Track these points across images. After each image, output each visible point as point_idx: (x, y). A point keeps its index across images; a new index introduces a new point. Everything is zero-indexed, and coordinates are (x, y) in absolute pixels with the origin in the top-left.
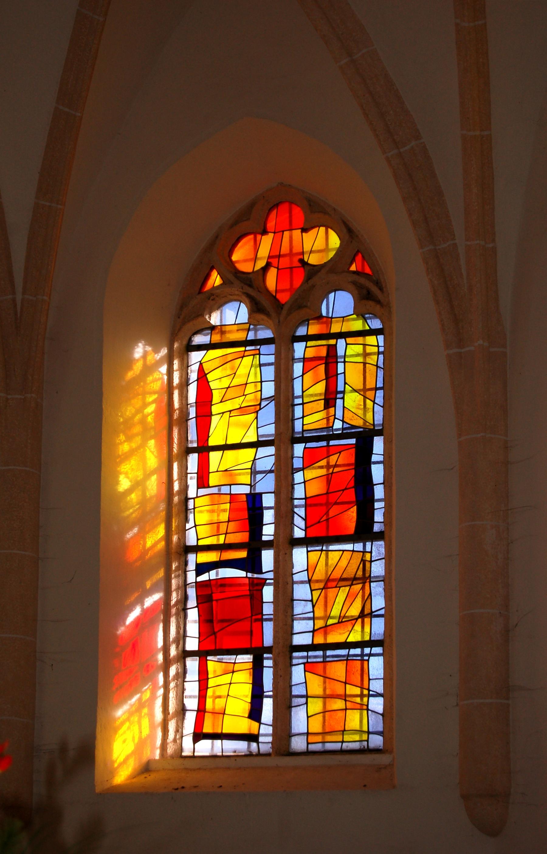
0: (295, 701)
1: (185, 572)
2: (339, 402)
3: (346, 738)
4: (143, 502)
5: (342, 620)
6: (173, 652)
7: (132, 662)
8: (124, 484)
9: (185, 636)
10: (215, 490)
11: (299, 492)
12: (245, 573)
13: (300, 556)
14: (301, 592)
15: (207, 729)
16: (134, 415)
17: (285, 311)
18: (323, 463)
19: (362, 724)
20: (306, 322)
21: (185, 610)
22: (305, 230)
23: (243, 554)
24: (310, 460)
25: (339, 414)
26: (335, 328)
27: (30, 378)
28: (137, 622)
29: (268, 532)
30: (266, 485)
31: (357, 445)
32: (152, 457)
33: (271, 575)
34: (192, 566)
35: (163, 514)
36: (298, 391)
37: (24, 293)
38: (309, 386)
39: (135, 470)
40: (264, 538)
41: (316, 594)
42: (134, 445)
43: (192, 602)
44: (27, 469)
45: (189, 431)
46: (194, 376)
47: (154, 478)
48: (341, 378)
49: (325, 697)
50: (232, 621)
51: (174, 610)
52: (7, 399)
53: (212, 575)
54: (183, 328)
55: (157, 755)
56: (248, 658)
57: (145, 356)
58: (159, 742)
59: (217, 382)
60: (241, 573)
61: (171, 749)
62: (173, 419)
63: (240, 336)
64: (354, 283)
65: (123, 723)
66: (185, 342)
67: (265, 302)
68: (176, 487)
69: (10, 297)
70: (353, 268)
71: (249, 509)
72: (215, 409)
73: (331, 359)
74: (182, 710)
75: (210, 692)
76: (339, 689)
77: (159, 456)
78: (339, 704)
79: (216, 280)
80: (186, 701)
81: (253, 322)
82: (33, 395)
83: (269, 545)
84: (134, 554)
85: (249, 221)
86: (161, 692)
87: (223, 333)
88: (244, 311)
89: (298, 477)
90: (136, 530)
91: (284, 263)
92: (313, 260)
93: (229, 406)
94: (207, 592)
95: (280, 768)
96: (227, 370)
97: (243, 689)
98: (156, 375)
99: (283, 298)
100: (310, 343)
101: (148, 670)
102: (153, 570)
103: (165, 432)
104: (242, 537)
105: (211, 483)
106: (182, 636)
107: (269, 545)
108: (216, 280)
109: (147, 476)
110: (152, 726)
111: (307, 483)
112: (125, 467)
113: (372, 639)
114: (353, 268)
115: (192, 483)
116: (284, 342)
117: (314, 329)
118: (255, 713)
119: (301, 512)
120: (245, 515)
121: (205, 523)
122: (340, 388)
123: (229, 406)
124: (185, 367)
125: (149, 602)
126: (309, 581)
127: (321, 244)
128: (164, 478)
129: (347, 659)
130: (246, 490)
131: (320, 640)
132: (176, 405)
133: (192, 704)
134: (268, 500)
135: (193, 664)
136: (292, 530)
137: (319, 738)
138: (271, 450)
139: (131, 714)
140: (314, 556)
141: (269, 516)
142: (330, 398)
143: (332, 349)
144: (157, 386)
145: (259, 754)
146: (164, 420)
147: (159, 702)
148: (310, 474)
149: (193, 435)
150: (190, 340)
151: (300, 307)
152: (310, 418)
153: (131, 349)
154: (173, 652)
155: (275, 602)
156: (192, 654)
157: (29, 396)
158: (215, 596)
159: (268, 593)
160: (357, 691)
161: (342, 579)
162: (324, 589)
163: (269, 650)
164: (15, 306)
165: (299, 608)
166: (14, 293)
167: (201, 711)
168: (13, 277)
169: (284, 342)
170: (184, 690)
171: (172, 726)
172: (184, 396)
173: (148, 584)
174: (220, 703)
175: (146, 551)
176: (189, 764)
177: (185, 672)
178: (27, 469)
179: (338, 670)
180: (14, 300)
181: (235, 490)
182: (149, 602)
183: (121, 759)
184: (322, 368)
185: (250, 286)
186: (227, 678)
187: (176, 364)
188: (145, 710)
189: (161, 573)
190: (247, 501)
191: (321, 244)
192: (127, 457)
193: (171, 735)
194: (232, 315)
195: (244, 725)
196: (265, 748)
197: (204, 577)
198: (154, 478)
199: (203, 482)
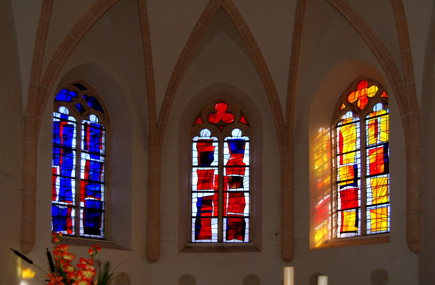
0: (367, 221)
1: (337, 189)
2: (378, 135)
3: (381, 230)
4: (323, 171)
5: (380, 197)
6: (334, 210)
7: (322, 215)
8: (317, 167)
9: (337, 206)
10: (345, 165)
11: (368, 162)
13: (368, 180)
14: (369, 190)
15: (344, 230)
16: (319, 148)
17: (363, 112)
18: (375, 153)
19: (385, 226)
20: (368, 114)
21: (337, 199)
22: (368, 88)
23: (352, 182)
24: (371, 152)
25: (378, 139)
26: (377, 114)
28: (322, 204)
29: (359, 175)
30: (359, 161)
31: (384, 147)
32: (326, 158)
33: (360, 187)
34: (339, 187)
35: (330, 174)
36: (367, 135)
38: (370, 132)
39: (320, 163)
40: (358, 177)
41: (373, 190)
42: (319, 156)
43: (339, 196)
45: (336, 150)
46: (338, 134)
47: (326, 164)
48: (379, 129)
49: (377, 219)
51: (334, 199)
53: (345, 188)
54: (335, 121)
55: (330, 238)
56: (355, 210)
57: (322, 131)
58: (330, 235)
59: (344, 135)
60: (352, 187)
61: (334, 237)
62: (332, 147)
63: (351, 121)
64: (382, 100)
65: (318, 231)
66: (335, 125)
67: (356, 110)
68: (334, 166)
70: (382, 96)
71: (354, 169)
72: (344, 143)
73: (376, 123)
74: (337, 226)
75: (344, 220)
76: (379, 216)
77: (328, 158)
78: (380, 220)
79: (344, 106)
80: (338, 223)
81: (354, 116)
83: (359, 178)
84: (320, 185)
86: (331, 221)
87: (346, 121)
88: (351, 113)
89: (368, 158)
90: (321, 179)
91: (362, 98)
92: (370, 96)
93: (347, 141)
94: (343, 193)
95: (365, 240)
96: (347, 131)
97: (353, 218)
98: (326, 136)
99: (362, 108)
100: (370, 120)
101: (326, 217)
102: (328, 189)
103: (330, 152)
104: (352, 177)
105: (344, 163)
106: (337, 206)
107: (359, 178)
108: (344, 106)
109: (324, 164)
110: (328, 231)
111: (370, 159)
112: (317, 163)
114: (382, 96)
115: (338, 164)
116: (363, 121)
117: (371, 116)
118: (356, 225)
119: (368, 168)
120: (353, 171)
121: (343, 174)
122: (379, 131)
123: (347, 141)
124: (336, 132)
125: (325, 198)
126: (371, 187)
127: (372, 91)
128: (330, 164)
129: (382, 207)
130: (353, 164)
131: (375, 203)
132: (333, 143)
133: (339, 224)
134: (359, 166)
135: (340, 213)
136: (366, 174)
137: (375, 230)
138: (359, 152)
139: (321, 228)
140: (372, 180)
141: (359, 170)
142: (376, 135)
143: (376, 121)
144: (327, 139)
145: (358, 236)
146: (330, 148)
147: (330, 224)
148: (370, 157)
149: (338, 151)
150: (337, 125)
151: (367, 110)
152: (371, 141)
153: (318, 130)
154: (334, 210)
155: (361, 194)
156: (339, 210)
158: (345, 194)
159: (359, 192)
161: (380, 186)
162: (377, 189)
163: (360, 207)
165: (368, 195)
167: (342, 226)
169: (363, 121)
170: (337, 220)
171: (334, 230)
172: (335, 140)
173: (325, 193)
174: (347, 223)
175: (324, 184)
176: (340, 240)
177: (338, 215)
179: (379, 211)
180: (284, 122)
181: (350, 164)
182: (325, 198)
183: (318, 240)
184: (373, 126)
185: (352, 106)
186: (348, 216)
187: (333, 132)
188: (325, 227)
189: (330, 190)
190: (354, 167)
192: (317, 160)
193: (334, 233)
194: (349, 115)
195: (354, 229)
196: (359, 234)
197: (341, 190)
198: (326, 164)
199: (341, 163)
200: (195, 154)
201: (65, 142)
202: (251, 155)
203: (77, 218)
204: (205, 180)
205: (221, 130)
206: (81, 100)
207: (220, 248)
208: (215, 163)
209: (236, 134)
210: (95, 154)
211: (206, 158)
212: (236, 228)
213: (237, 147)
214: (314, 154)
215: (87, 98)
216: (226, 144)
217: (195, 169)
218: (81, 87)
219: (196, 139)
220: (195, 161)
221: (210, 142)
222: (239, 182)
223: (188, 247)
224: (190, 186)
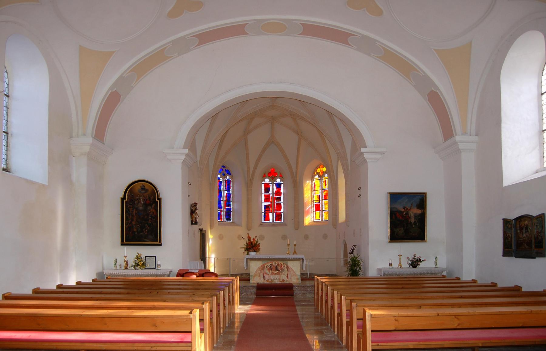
7: (308, 212)
17: (321, 176)
45: (313, 189)
50: (318, 208)
54: (312, 178)
62: (312, 188)
85: (318, 167)
111: (324, 194)
121: (315, 198)
127: (324, 169)
191: (324, 169)
194: (317, 177)
200: (263, 188)
201: (253, 287)
202: (284, 189)
203: (223, 215)
204: (267, 198)
205: (273, 179)
206: (224, 172)
207: (273, 224)
208: (271, 192)
209: (278, 181)
210: (229, 191)
211: (267, 190)
212: (278, 217)
213: (278, 186)
214: (320, 348)
215: (226, 170)
216: (274, 185)
217: (263, 194)
218: (224, 167)
219: (263, 182)
220: (263, 191)
221: (269, 184)
222: (279, 199)
223: (262, 224)
224: (262, 201)
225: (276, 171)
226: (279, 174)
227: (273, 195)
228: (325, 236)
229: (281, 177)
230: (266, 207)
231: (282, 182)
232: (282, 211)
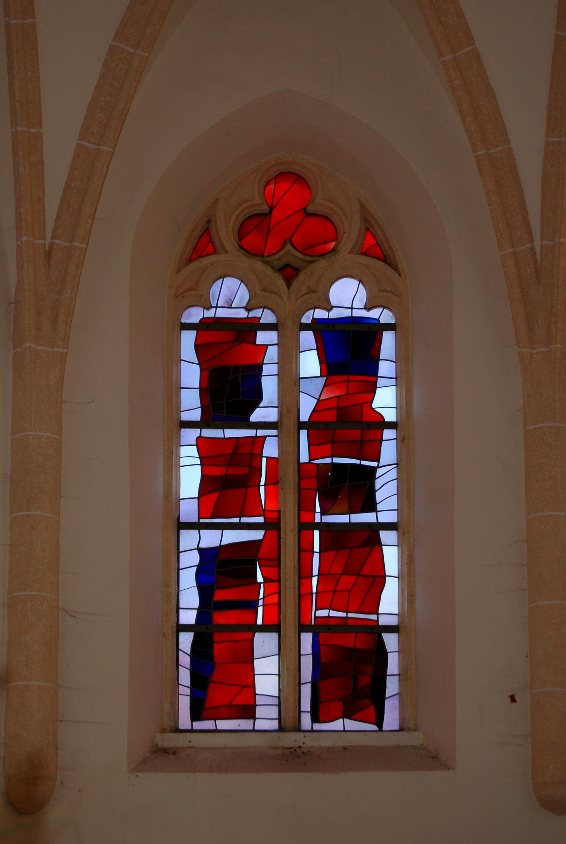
12: (317, 574)
27: (554, 328)
37: (542, 239)
44: (557, 424)
52: (532, 354)
69: (528, 245)
82: (558, 345)
113: (221, 531)
157: (553, 347)
160: (545, 503)
164: (534, 254)
166: (532, 241)
168: (530, 224)
178: (557, 424)
180: (532, 249)
200: (191, 374)
202: (402, 380)
204: (230, 481)
208: (264, 413)
209: (347, 296)
211: (231, 390)
212: (349, 673)
213: (350, 350)
216: (307, 338)
220: (191, 404)
221: (246, 329)
222: (358, 488)
225: (319, 204)
226: (351, 234)
227: (289, 446)
228: (137, 776)
229: (377, 256)
230: (213, 565)
231: (385, 316)
232: (390, 601)
